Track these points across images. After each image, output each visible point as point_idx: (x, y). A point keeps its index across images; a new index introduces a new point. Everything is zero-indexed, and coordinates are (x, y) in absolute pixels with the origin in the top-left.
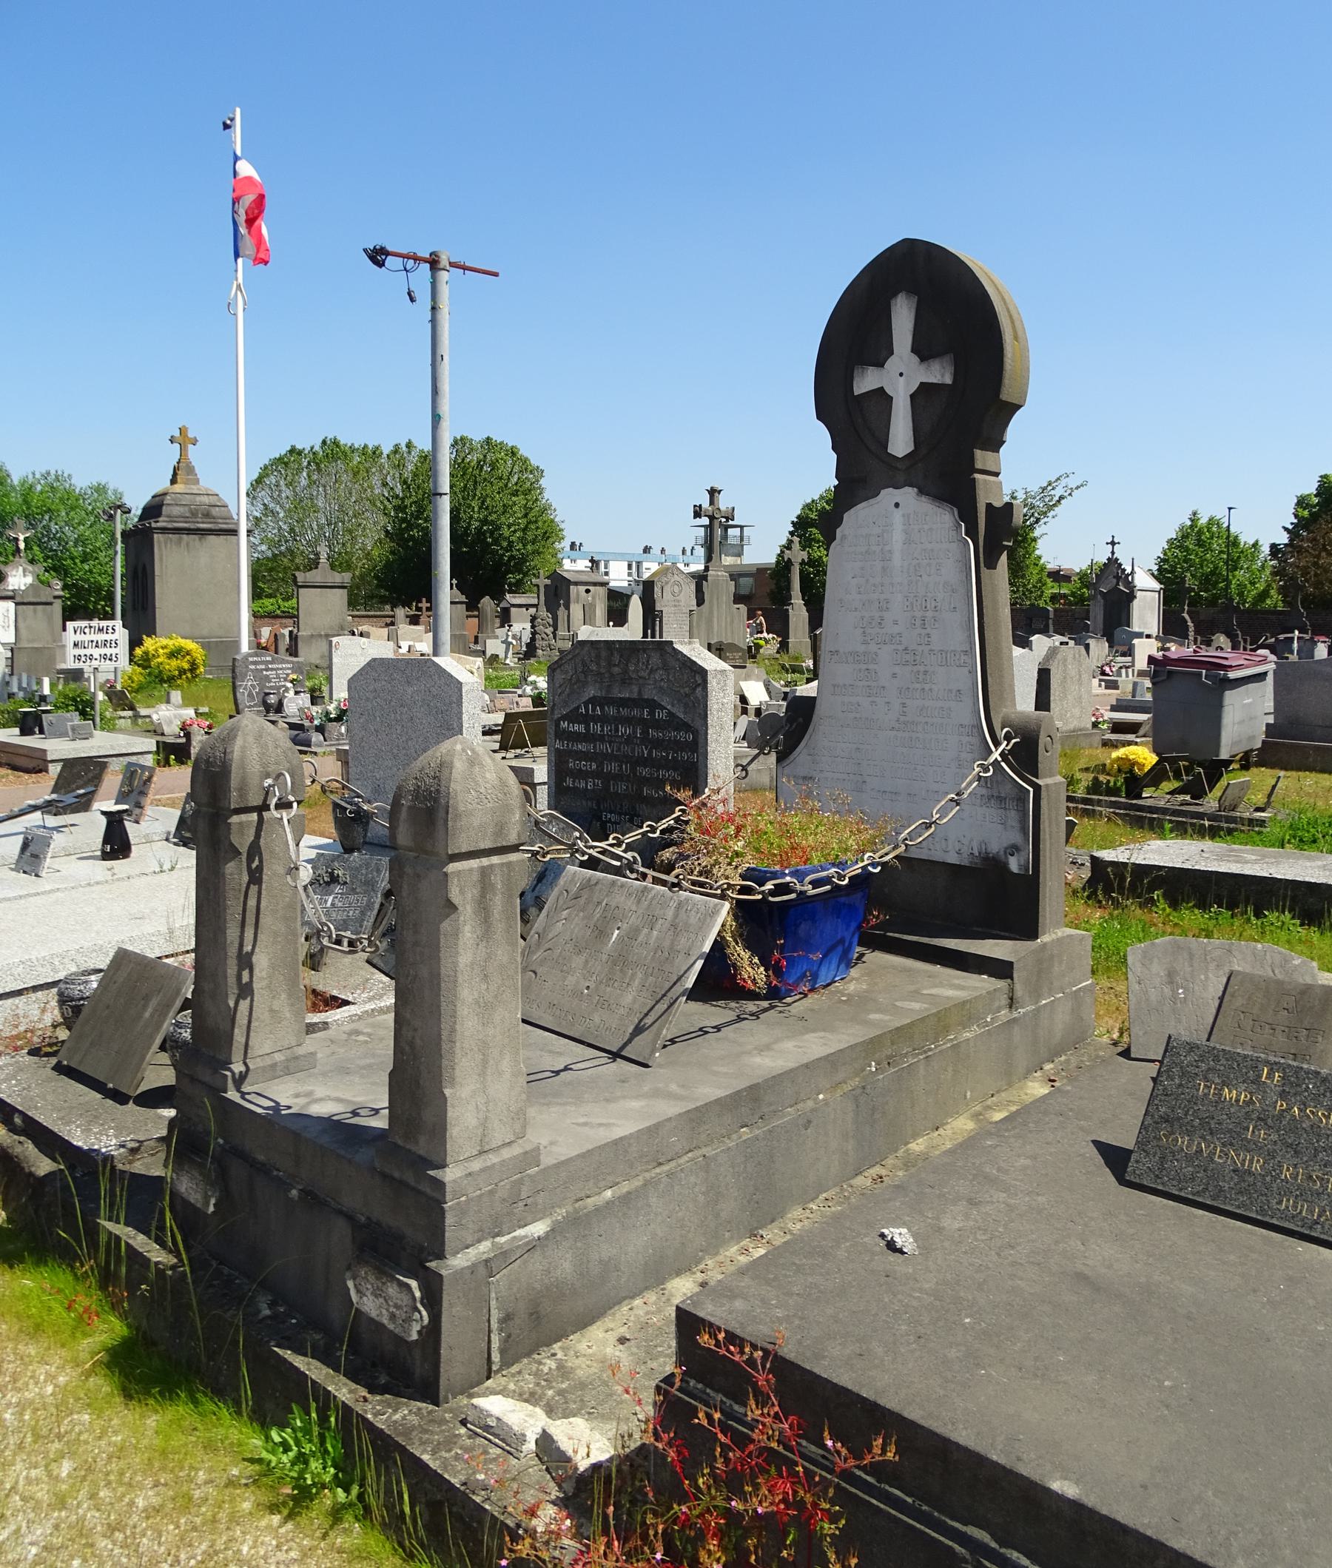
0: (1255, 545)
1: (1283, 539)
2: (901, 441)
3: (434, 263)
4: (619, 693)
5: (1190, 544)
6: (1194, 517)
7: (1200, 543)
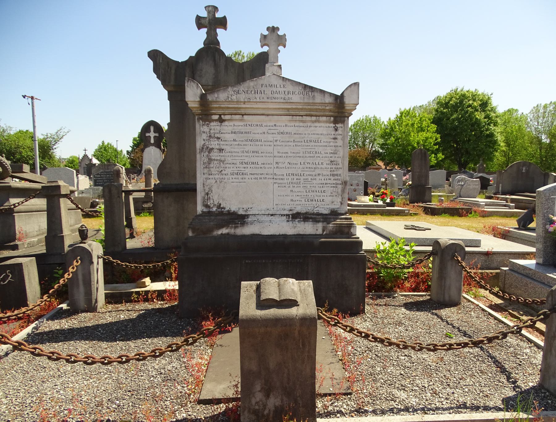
0: (121, 151)
1: (130, 149)
2: (152, 141)
3: (32, 98)
4: (106, 171)
5: (102, 150)
6: (103, 142)
7: (105, 150)
